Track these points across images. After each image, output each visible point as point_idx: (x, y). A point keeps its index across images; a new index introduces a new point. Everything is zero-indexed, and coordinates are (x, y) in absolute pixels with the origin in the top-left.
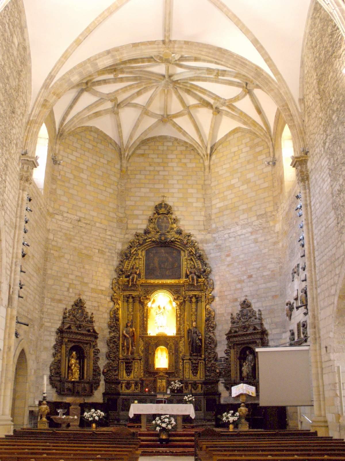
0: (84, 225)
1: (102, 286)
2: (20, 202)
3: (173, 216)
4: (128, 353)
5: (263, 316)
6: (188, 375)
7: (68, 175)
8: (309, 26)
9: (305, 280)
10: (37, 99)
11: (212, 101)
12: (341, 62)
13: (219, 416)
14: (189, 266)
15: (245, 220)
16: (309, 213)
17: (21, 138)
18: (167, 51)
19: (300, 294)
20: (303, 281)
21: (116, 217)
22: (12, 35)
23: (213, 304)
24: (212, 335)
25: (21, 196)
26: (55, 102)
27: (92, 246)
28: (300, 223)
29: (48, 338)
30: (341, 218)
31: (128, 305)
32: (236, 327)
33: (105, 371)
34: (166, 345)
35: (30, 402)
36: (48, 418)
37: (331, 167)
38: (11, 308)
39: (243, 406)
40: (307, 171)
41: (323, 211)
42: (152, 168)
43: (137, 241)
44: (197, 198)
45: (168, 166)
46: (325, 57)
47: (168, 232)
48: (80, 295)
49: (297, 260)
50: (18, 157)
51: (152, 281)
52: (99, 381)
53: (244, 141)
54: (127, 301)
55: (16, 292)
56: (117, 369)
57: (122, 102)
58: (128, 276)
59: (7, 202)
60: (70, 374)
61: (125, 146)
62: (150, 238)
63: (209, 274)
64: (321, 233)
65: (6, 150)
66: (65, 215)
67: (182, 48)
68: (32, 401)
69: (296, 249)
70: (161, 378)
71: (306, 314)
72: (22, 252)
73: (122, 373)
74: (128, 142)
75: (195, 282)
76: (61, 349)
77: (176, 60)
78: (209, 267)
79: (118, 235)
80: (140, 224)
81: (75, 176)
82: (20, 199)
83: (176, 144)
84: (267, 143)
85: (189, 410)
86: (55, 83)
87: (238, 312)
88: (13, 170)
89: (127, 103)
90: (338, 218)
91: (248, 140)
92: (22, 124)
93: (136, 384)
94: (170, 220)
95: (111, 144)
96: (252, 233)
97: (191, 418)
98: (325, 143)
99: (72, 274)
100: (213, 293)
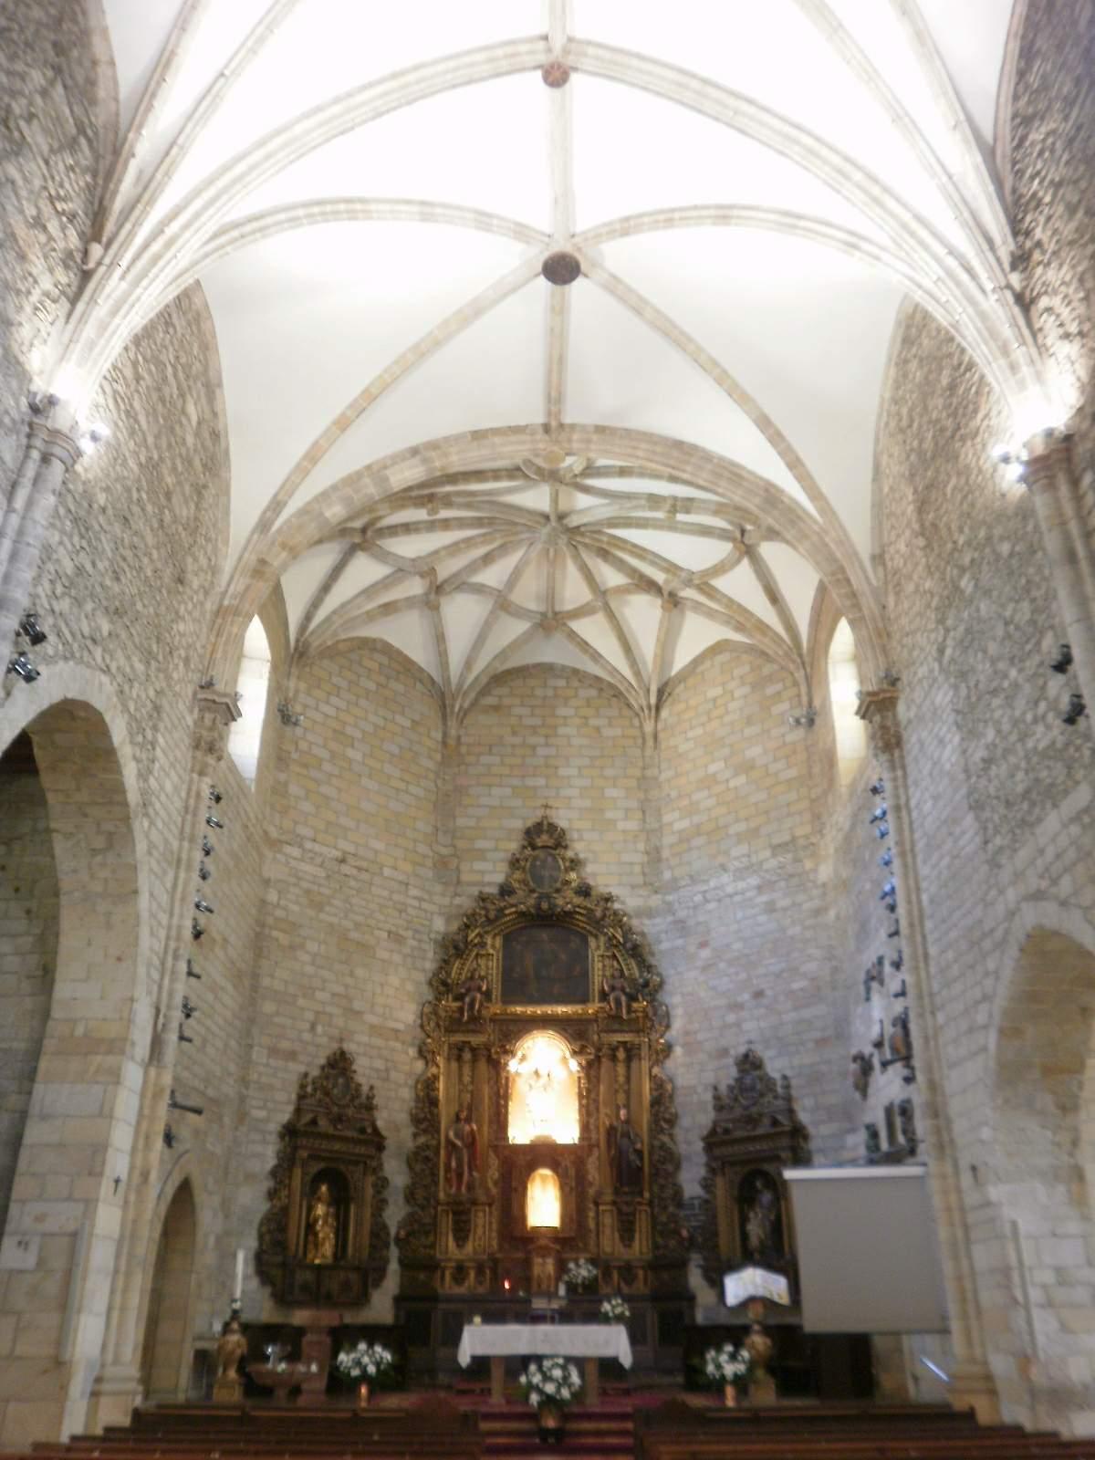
0: (355, 872)
1: (396, 1020)
2: (192, 802)
3: (570, 854)
4: (459, 1188)
5: (794, 1093)
6: (610, 1243)
7: (315, 750)
8: (890, 382)
9: (903, 994)
10: (240, 558)
11: (659, 577)
12: (979, 447)
13: (696, 1361)
14: (608, 973)
15: (744, 860)
16: (906, 827)
17: (198, 646)
18: (556, 448)
19: (889, 1030)
20: (897, 996)
21: (431, 854)
22: (182, 395)
23: (669, 1064)
24: (665, 1139)
25: (194, 788)
26: (284, 567)
27: (373, 922)
28: (882, 854)
29: (258, 1148)
30: (995, 827)
31: (460, 1068)
32: (727, 1121)
33: (403, 1233)
34: (555, 1166)
35: (199, 1325)
36: (241, 1370)
37: (960, 706)
38: (158, 1067)
39: (758, 1332)
40: (897, 724)
41: (943, 817)
42: (517, 740)
43: (483, 912)
44: (627, 810)
45: (556, 735)
46: (936, 444)
47: (558, 891)
48: (341, 1040)
49: (879, 945)
50: (190, 693)
51: (519, 1009)
52: (386, 1261)
53: (737, 672)
54: (459, 1058)
55: (175, 1025)
56: (433, 1229)
57: (446, 581)
58: (459, 998)
59: (158, 798)
60: (311, 1246)
61: (454, 687)
62: (512, 906)
63: (656, 991)
64: (940, 873)
65: (159, 670)
66: (309, 845)
67: (589, 441)
68: (206, 1321)
69: (873, 921)
70: (544, 1251)
71: (909, 1080)
72: (194, 927)
73: (444, 1239)
74: (462, 677)
75: (624, 1011)
76: (290, 1178)
77: (576, 476)
78: (659, 974)
79: (437, 899)
80: (490, 872)
81: (333, 754)
82: (193, 794)
83: (576, 684)
84: (792, 674)
85: (613, 1342)
86: (288, 521)
87: (732, 1082)
88: (176, 722)
89: (458, 583)
90: (985, 829)
91: (747, 668)
92: (203, 613)
93: (480, 1270)
94: (561, 862)
95: (421, 681)
96: (759, 888)
97: (621, 1366)
98: (941, 651)
99: (323, 990)
100: (668, 1036)
